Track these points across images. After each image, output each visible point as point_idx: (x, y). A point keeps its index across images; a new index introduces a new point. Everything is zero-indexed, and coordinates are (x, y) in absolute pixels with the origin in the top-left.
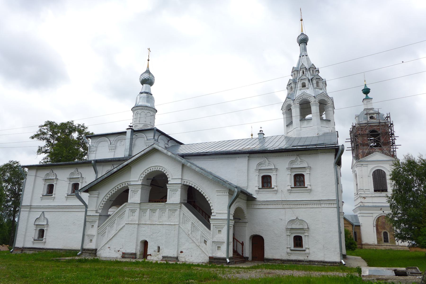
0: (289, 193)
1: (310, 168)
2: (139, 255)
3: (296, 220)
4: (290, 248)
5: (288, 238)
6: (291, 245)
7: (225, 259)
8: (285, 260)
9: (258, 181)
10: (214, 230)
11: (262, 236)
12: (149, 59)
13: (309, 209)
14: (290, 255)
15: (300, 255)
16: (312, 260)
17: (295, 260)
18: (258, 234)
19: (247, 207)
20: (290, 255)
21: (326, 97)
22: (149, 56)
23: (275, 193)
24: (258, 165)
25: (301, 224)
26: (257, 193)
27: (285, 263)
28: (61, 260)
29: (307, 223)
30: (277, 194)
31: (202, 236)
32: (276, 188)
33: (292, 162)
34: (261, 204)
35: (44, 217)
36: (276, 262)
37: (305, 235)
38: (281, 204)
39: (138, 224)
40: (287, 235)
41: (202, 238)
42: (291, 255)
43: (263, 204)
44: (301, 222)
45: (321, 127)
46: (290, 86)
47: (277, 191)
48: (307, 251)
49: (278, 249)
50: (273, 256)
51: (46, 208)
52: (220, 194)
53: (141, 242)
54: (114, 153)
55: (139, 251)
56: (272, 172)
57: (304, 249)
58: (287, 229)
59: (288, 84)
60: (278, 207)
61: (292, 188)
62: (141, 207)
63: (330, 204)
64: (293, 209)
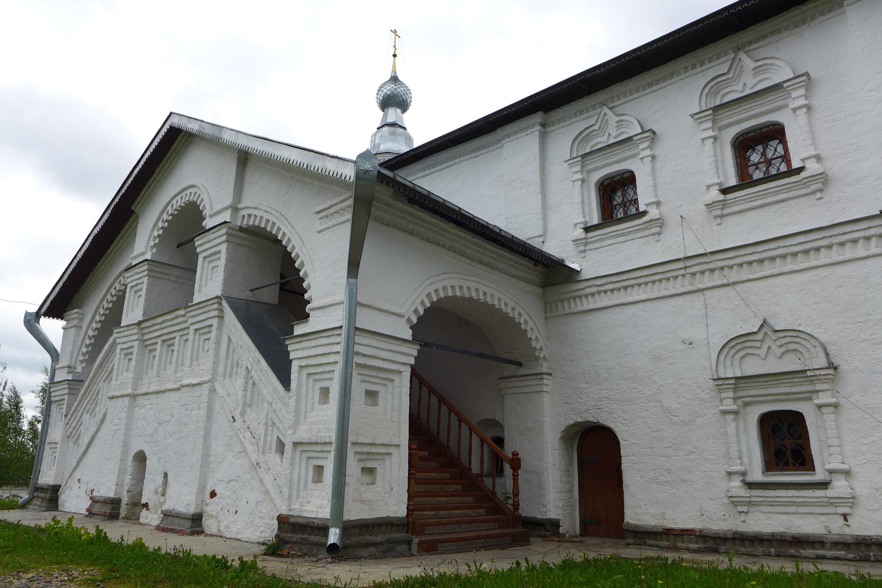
0: (716, 217)
1: (804, 78)
2: (127, 505)
3: (760, 336)
4: (744, 474)
5: (731, 428)
6: (750, 457)
7: (323, 529)
8: (722, 536)
9: (583, 201)
10: (304, 389)
11: (611, 425)
12: (396, 53)
13: (828, 270)
14: (745, 509)
15: (801, 510)
16: (871, 538)
17: (773, 535)
18: (592, 419)
19: (546, 312)
20: (745, 509)
22: (394, 47)
23: (654, 234)
24: (578, 140)
25: (788, 351)
26: (581, 252)
27: (723, 548)
29: (823, 340)
30: (662, 237)
31: (270, 423)
33: (715, 85)
34: (599, 293)
36: (680, 544)
37: (816, 401)
38: (684, 276)
39: (134, 397)
40: (725, 413)
41: (270, 429)
42: (752, 509)
43: (606, 292)
44: (788, 340)
47: (660, 222)
48: (840, 487)
49: (685, 481)
50: (664, 514)
52: (334, 222)
53: (136, 461)
55: (128, 492)
56: (636, 155)
57: (819, 475)
58: (720, 382)
60: (673, 292)
62: (146, 337)
64: (740, 286)
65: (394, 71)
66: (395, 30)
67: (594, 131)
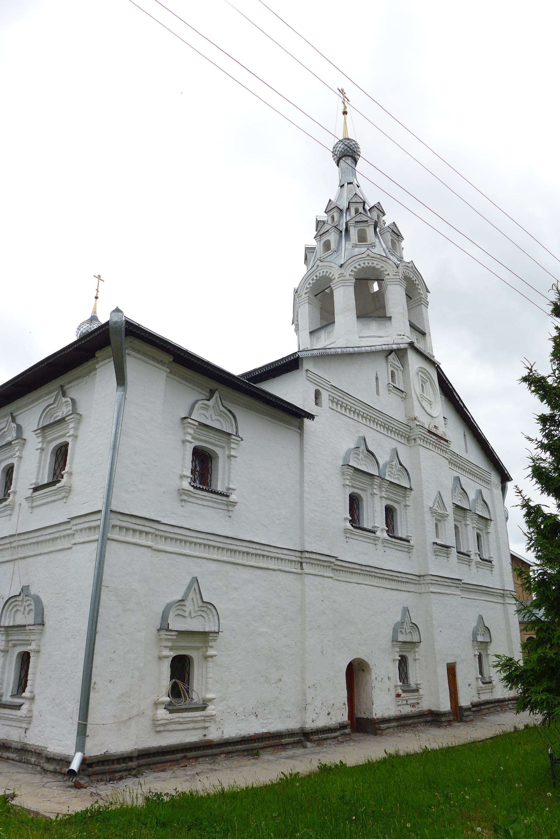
3: (20, 598)
12: (98, 296)
21: (378, 259)
22: (97, 290)
28: (17, 758)
45: (360, 337)
59: (326, 209)
65: (94, 312)
66: (99, 276)
67: (5, 432)
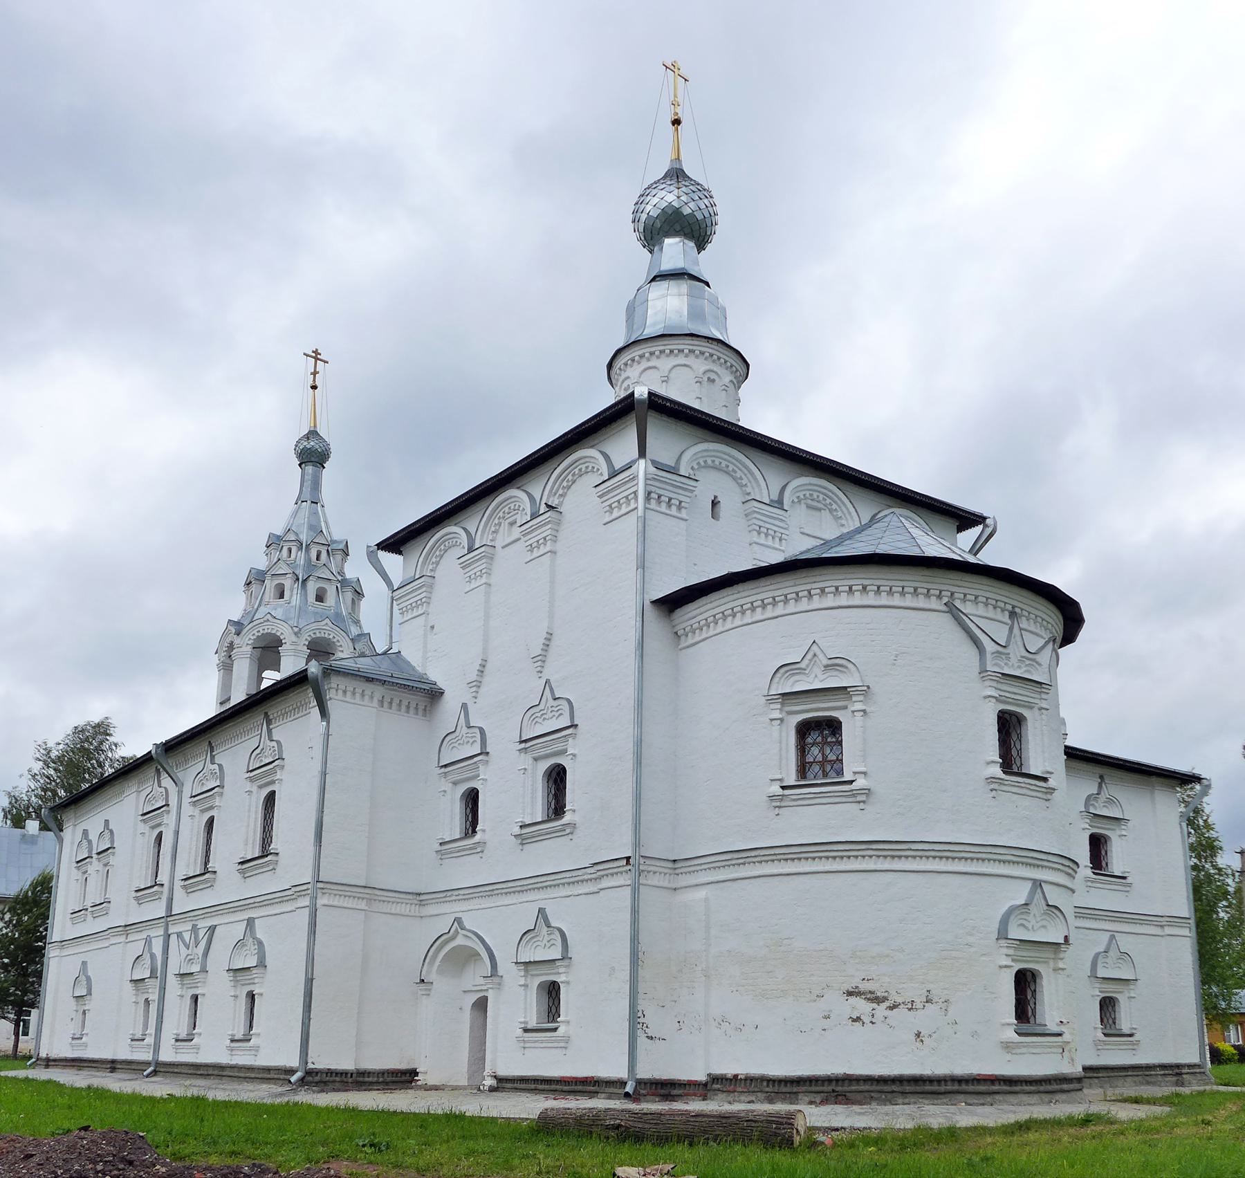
23: (859, 802)
32: (861, 782)
35: (549, 926)
46: (279, 582)
47: (868, 792)
51: (262, 905)
54: (488, 594)
57: (847, 776)
61: (783, 788)
63: (352, 898)
66: (316, 352)
